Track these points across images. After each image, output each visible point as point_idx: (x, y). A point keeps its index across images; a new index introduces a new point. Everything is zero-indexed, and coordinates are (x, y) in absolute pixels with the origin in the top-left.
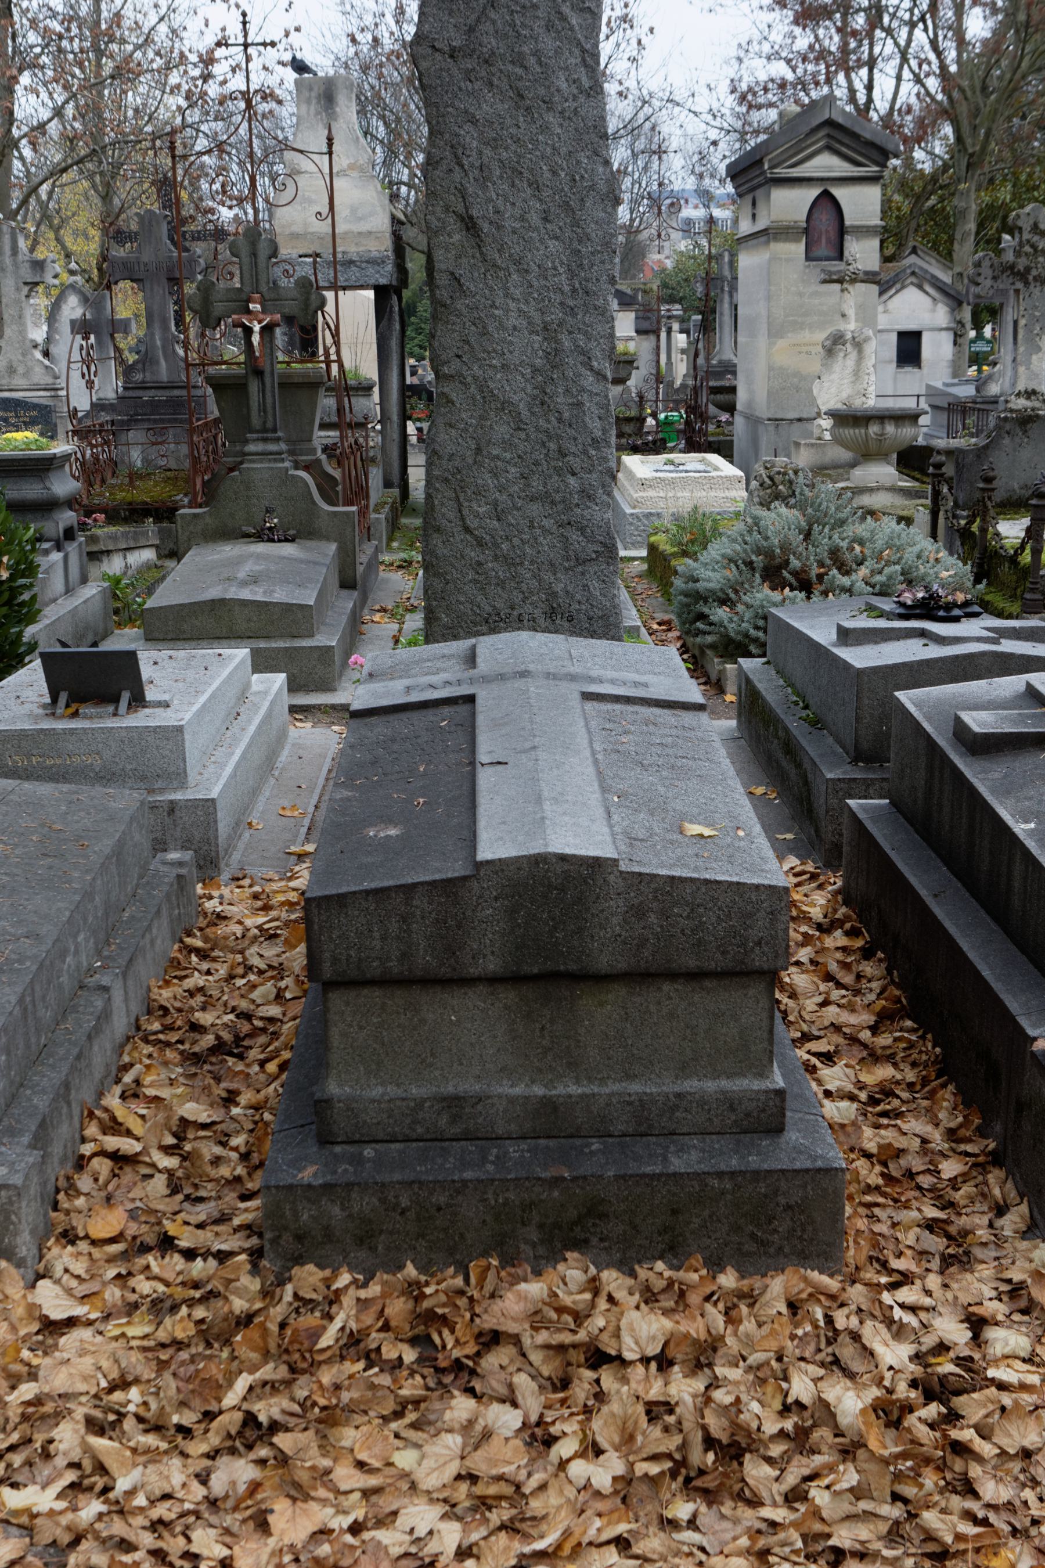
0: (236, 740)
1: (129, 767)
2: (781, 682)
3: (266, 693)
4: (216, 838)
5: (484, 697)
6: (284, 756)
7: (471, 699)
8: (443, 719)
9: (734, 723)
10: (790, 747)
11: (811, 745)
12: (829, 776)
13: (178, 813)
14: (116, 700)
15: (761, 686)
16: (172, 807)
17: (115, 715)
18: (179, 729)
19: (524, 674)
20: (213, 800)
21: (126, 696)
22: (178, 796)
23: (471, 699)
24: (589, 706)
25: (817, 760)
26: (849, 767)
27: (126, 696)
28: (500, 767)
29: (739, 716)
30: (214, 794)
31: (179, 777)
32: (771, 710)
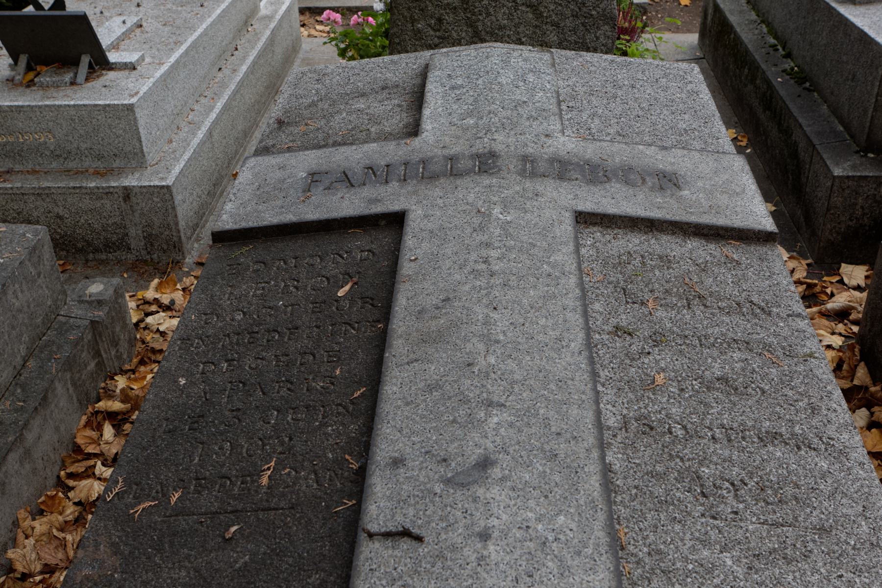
0: (223, 85)
1: (84, 146)
2: (753, 16)
3: (269, 18)
4: (177, 224)
5: (428, 214)
6: (297, 68)
7: (396, 221)
8: (359, 245)
9: (693, 38)
10: (769, 99)
11: (808, 121)
12: (837, 172)
13: (134, 200)
14: (75, 63)
15: (733, 19)
16: (127, 193)
17: (73, 83)
18: (130, 108)
19: (486, 163)
20: (168, 187)
21: (85, 60)
22: (131, 181)
23: (396, 221)
24: (595, 236)
25: (816, 141)
26: (856, 159)
27: (85, 60)
28: (405, 544)
29: (703, 34)
30: (169, 182)
31: (136, 158)
32: (747, 51)
